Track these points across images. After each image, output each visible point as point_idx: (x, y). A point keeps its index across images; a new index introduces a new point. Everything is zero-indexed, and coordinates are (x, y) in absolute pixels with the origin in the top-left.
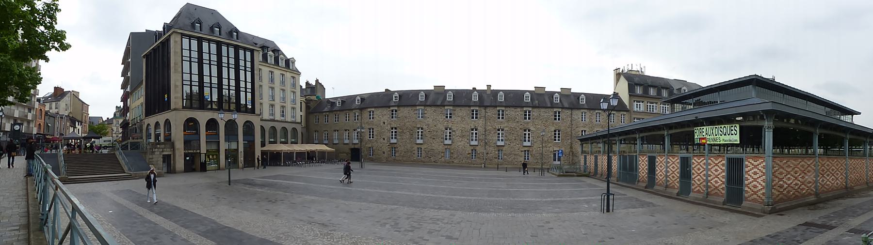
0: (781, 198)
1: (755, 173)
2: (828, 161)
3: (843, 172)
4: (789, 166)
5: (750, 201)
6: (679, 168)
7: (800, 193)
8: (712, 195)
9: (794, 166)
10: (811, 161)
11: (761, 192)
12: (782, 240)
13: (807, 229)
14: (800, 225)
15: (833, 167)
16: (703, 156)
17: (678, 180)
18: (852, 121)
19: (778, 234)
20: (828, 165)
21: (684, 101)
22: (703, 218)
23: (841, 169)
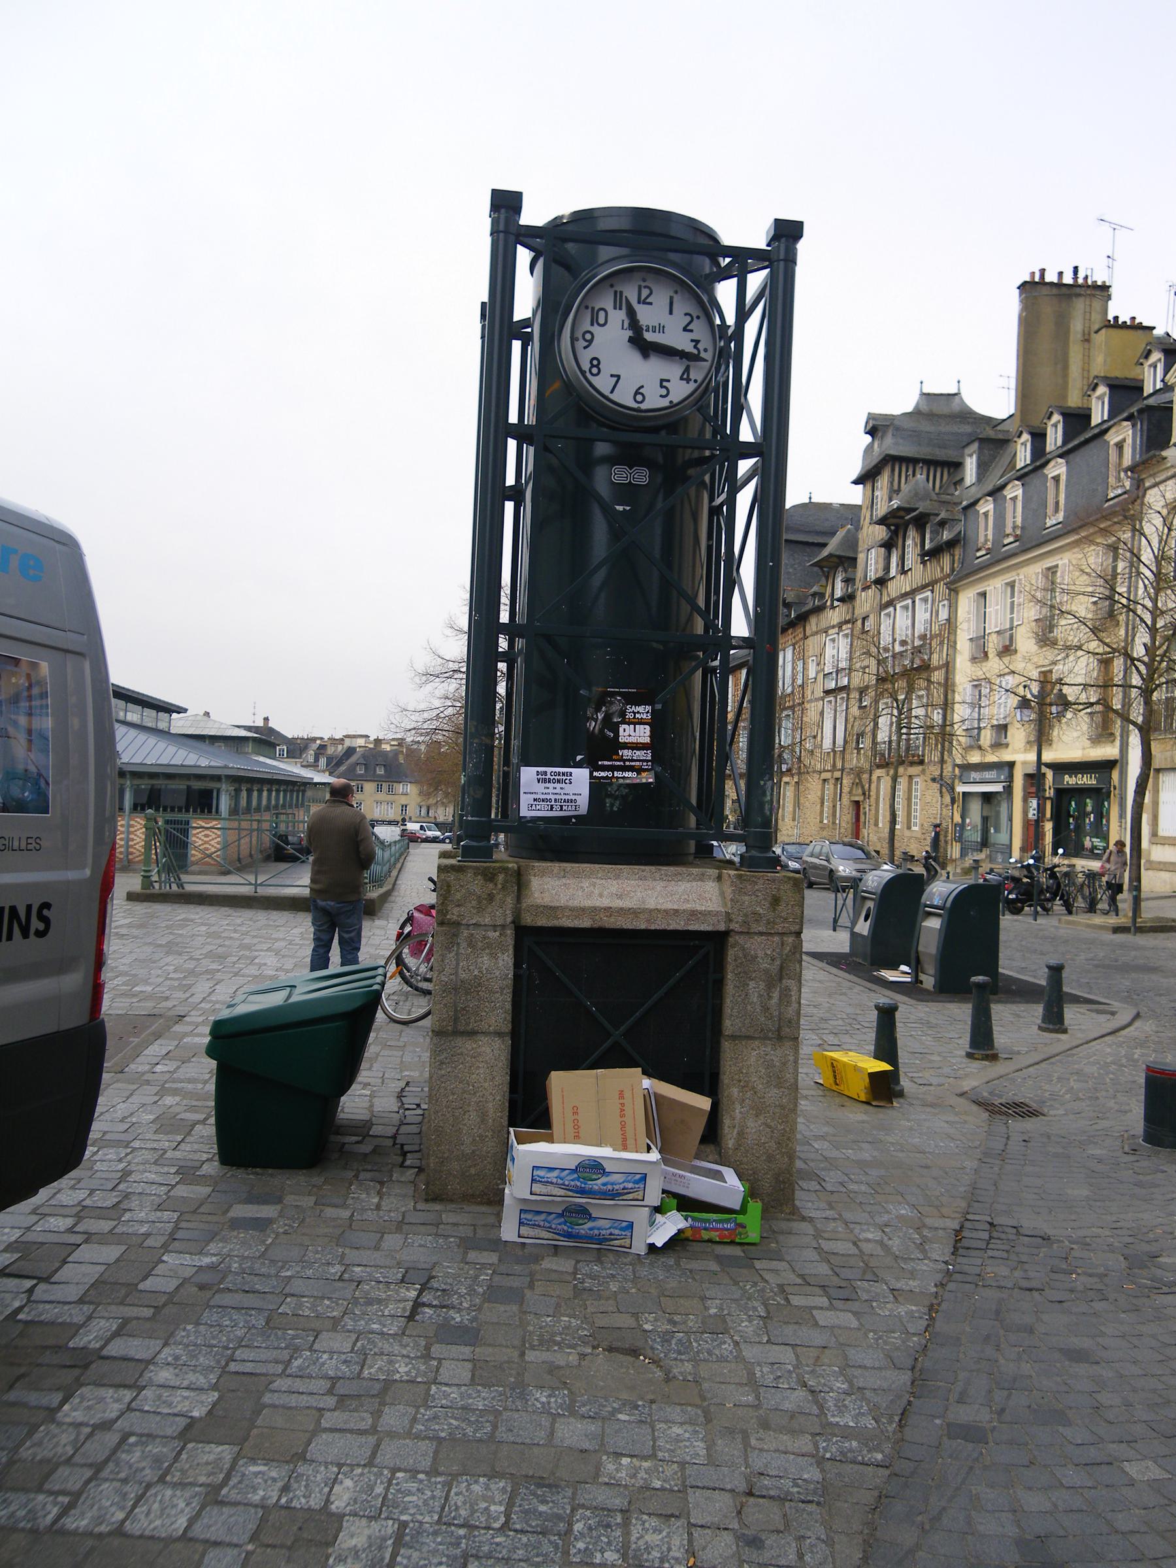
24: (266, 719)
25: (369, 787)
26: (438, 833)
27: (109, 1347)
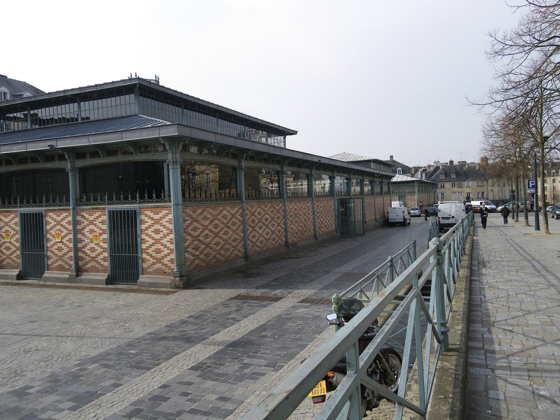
0: (198, 265)
1: (157, 232)
2: (259, 207)
3: (281, 222)
4: (206, 218)
5: (150, 273)
6: (20, 233)
7: (223, 256)
8: (87, 271)
9: (213, 218)
10: (236, 209)
11: (169, 258)
12: (210, 320)
13: (243, 303)
14: (231, 298)
15: (267, 216)
16: (67, 210)
17: (18, 252)
18: (285, 145)
19: (203, 313)
20: (259, 213)
21: (11, 115)
22: (80, 306)
23: (278, 218)
24: (392, 157)
25: (448, 185)
26: (494, 207)
27: (501, 381)
